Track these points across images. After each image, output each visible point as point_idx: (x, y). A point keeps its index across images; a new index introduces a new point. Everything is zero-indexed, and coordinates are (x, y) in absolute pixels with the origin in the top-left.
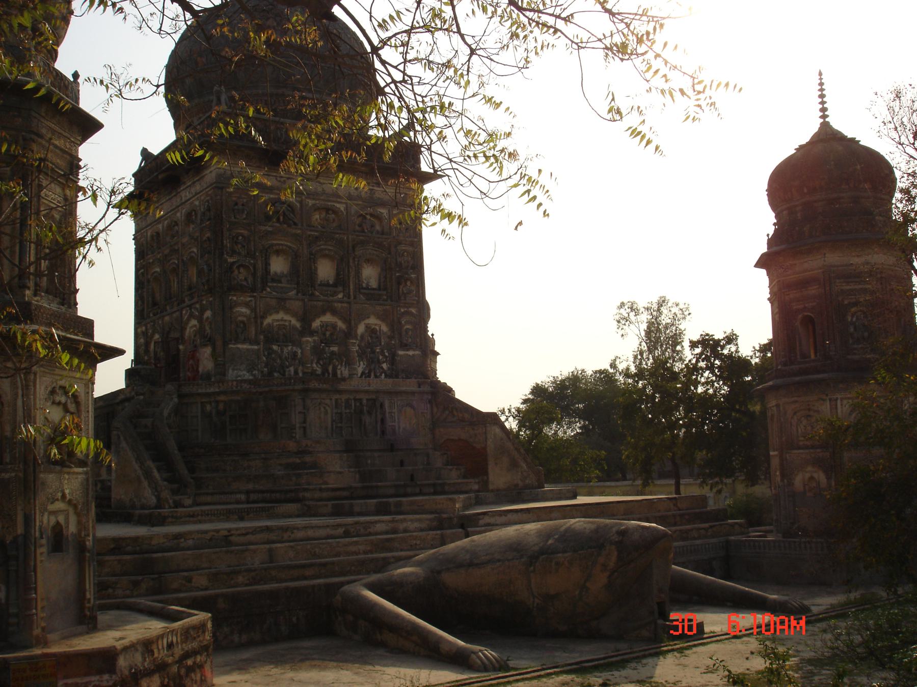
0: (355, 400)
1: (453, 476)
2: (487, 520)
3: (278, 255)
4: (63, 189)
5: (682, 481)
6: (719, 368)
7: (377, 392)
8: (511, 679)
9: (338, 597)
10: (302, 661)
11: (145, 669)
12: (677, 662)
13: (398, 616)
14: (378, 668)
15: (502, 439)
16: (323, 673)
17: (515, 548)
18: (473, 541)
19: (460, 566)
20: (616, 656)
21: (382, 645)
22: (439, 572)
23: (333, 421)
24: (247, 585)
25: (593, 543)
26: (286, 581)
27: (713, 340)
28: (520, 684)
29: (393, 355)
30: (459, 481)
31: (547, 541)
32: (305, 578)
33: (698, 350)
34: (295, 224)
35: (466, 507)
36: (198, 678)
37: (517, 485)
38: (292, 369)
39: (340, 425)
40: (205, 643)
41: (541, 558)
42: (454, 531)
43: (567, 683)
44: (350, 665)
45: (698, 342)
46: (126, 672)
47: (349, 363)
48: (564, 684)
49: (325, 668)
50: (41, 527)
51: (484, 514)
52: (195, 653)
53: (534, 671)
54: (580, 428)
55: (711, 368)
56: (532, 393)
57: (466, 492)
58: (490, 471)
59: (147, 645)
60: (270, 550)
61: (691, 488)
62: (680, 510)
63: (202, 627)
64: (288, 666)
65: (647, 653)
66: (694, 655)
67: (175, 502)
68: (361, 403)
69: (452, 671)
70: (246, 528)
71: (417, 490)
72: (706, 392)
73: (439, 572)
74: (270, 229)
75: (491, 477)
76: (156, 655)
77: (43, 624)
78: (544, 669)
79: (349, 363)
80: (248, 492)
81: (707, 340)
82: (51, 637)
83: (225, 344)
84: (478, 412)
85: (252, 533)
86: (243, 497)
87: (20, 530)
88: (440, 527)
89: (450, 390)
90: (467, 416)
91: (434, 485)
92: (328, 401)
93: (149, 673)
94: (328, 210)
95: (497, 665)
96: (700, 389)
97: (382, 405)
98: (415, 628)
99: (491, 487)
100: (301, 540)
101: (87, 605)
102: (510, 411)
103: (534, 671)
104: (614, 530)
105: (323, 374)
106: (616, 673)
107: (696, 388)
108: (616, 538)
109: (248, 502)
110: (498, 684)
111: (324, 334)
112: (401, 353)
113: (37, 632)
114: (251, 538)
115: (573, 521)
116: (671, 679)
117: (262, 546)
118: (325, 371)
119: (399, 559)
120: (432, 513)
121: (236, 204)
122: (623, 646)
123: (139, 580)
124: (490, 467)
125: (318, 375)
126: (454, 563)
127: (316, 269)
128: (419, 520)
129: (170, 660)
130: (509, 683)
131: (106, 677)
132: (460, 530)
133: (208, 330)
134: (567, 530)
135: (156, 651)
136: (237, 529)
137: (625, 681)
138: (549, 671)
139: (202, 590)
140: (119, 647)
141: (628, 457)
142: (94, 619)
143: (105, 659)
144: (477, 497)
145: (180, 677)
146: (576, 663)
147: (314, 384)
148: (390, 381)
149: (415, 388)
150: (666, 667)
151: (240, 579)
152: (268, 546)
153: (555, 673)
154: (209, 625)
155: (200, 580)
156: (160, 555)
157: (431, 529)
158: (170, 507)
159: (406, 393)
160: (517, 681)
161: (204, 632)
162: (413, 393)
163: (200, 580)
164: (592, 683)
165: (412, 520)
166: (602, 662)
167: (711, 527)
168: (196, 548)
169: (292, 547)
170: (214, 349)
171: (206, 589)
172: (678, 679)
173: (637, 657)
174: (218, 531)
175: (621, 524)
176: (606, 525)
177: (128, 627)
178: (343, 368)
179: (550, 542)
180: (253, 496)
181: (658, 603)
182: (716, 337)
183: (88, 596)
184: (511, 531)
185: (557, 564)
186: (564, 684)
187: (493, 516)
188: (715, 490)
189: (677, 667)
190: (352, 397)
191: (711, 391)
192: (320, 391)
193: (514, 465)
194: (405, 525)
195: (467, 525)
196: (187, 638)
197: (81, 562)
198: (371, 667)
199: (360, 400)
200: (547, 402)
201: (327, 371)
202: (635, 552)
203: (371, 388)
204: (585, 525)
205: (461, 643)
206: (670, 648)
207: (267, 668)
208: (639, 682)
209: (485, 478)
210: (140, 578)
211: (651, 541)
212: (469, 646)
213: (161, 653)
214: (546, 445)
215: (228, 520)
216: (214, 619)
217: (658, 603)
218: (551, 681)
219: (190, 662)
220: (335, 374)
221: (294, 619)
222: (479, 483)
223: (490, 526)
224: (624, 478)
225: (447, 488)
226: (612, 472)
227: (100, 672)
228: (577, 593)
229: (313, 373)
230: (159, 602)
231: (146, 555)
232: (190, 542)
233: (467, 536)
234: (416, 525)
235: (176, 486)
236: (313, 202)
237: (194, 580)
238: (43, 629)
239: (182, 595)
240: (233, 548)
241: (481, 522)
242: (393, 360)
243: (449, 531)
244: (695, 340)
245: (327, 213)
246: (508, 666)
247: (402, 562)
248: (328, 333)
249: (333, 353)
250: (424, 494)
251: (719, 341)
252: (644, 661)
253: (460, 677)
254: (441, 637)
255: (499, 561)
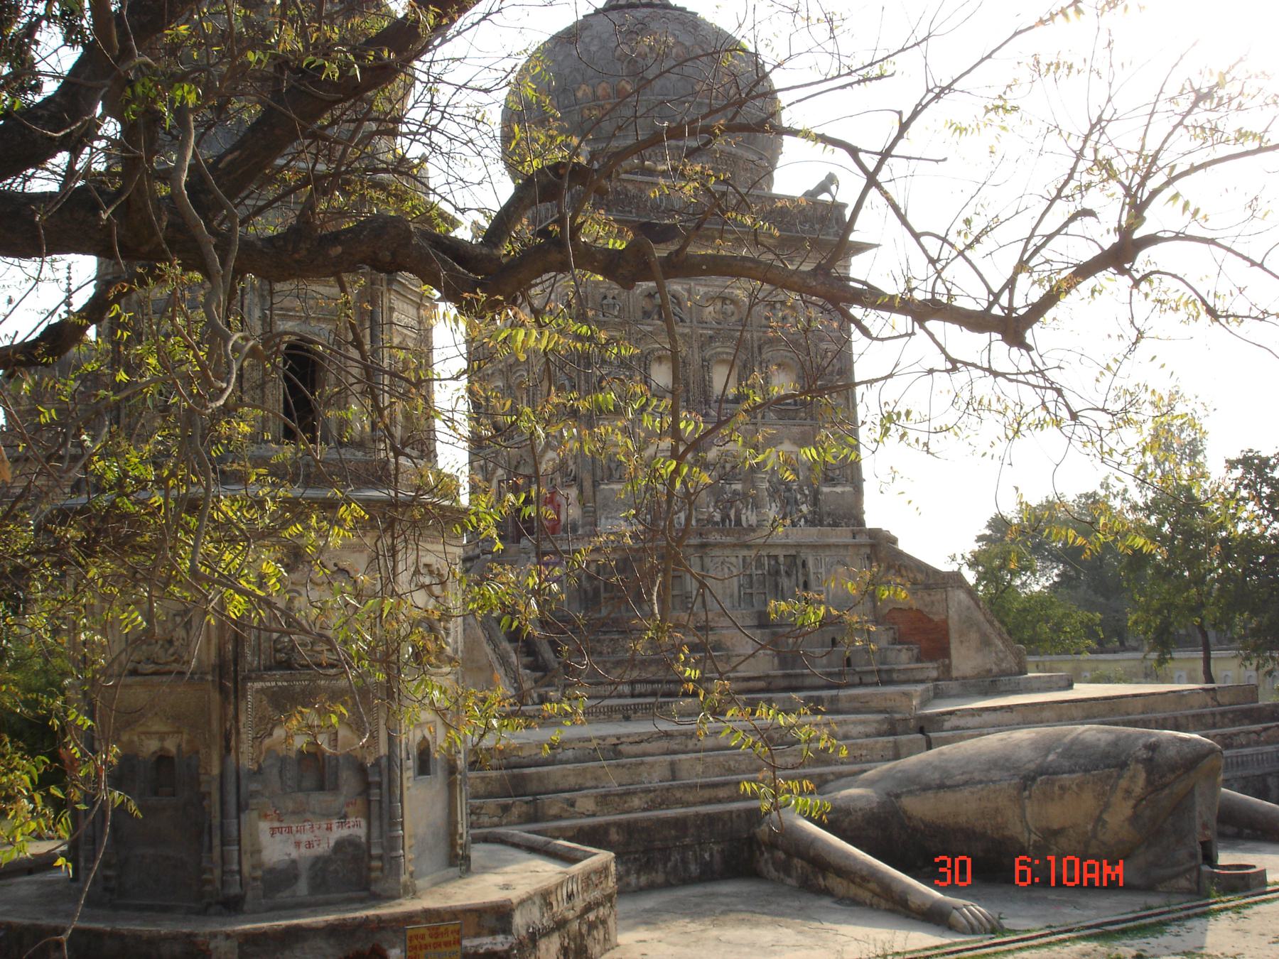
0: (769, 556)
1: (903, 658)
2: (954, 721)
3: (660, 362)
4: (418, 309)
5: (1213, 654)
6: (1268, 497)
7: (799, 545)
8: (1012, 946)
9: (764, 828)
10: (724, 913)
11: (545, 928)
12: (1234, 926)
13: (848, 856)
14: (827, 925)
15: (969, 608)
16: (756, 932)
17: (1001, 762)
18: (941, 753)
19: (926, 788)
20: (1149, 916)
21: (827, 892)
22: (898, 796)
23: (740, 586)
24: (644, 810)
25: (1110, 762)
26: (694, 804)
27: (1259, 458)
28: (1025, 954)
29: (816, 493)
30: (912, 666)
31: (1046, 756)
32: (719, 801)
33: (1238, 473)
34: (682, 321)
35: (924, 704)
36: (601, 937)
37: (990, 671)
38: (682, 515)
39: (749, 591)
40: (609, 891)
41: (1039, 779)
42: (911, 736)
43: (1088, 954)
44: (789, 920)
45: (1239, 461)
46: (523, 933)
47: (757, 505)
48: (1084, 955)
49: (757, 925)
50: (407, 744)
51: (951, 713)
52: (598, 904)
53: (1042, 936)
54: (1057, 575)
55: (1258, 498)
56: (989, 526)
57: (922, 681)
58: (953, 652)
59: (545, 897)
60: (672, 764)
61: (1231, 670)
62: (1219, 705)
63: (603, 871)
64: (707, 921)
65: (1191, 912)
66: (1256, 917)
67: (540, 696)
68: (777, 562)
69: (927, 932)
70: (639, 734)
71: (857, 680)
72: (1250, 531)
73: (898, 796)
74: (650, 329)
75: (955, 661)
76: (555, 909)
77: (411, 868)
78: (1053, 934)
79: (757, 505)
80: (632, 683)
81: (1250, 458)
82: (420, 883)
83: (595, 484)
84: (936, 572)
85: (648, 741)
86: (626, 689)
87: (383, 749)
88: (892, 732)
89: (880, 530)
90: (920, 577)
91: (879, 671)
92: (733, 560)
93: (547, 933)
94: (724, 299)
95: (988, 927)
96: (1241, 527)
97: (804, 564)
98: (874, 874)
99: (954, 674)
100: (712, 750)
101: (459, 841)
102: (963, 558)
103: (1042, 936)
104: (1141, 742)
105: (723, 520)
106: (1151, 940)
107: (1235, 526)
108: (1144, 754)
109: (633, 696)
110: (996, 953)
111: (724, 467)
112: (825, 490)
113: (404, 878)
114: (645, 747)
115: (1081, 728)
116: (1230, 951)
117: (661, 758)
118: (726, 517)
119: (839, 776)
120: (880, 712)
121: (605, 297)
122: (1154, 900)
123: (514, 801)
124: (953, 646)
125: (717, 523)
126: (919, 784)
127: (711, 381)
128: (863, 722)
129: (570, 915)
130: (1009, 951)
131: (500, 938)
132: (920, 736)
133: (572, 466)
134: (1073, 742)
135: (555, 903)
136: (628, 736)
137: (1166, 951)
138: (1061, 936)
139: (588, 816)
140: (515, 901)
141: (1136, 623)
142: (467, 859)
143: (499, 916)
144: (936, 687)
145: (582, 936)
146: (1097, 926)
147: (714, 537)
148: (814, 530)
149: (849, 540)
150: (1219, 932)
151: (636, 802)
152: (668, 758)
153: (1069, 939)
154: (613, 867)
155: (585, 803)
156: (533, 770)
157: (880, 734)
158: (534, 704)
159: (837, 546)
160: (1020, 949)
161: (606, 877)
162: (846, 546)
163: (585, 803)
164: (1122, 955)
165: (854, 723)
166: (1131, 924)
167: (1265, 729)
168: (577, 760)
169: (699, 759)
170: (581, 492)
171: (594, 815)
172: (1238, 951)
173: (1179, 919)
174: (604, 738)
175: (1150, 735)
176: (1129, 736)
177: (509, 869)
178: (749, 513)
179: (1051, 757)
180: (639, 688)
181: (1203, 844)
182: (1263, 455)
183: (460, 830)
184: (992, 742)
185: (1061, 787)
186: (1084, 955)
187: (962, 716)
188: (1262, 671)
189: (1236, 934)
190: (764, 553)
191: (1257, 531)
192: (723, 546)
193: (986, 642)
194: (845, 728)
195: (927, 730)
196: (588, 885)
197: (451, 786)
198: (816, 924)
199: (776, 557)
200: (1009, 542)
201: (728, 517)
202: (1169, 775)
203: (789, 541)
204: (1099, 736)
205: (937, 895)
206: (1222, 905)
207: (681, 922)
208: (1185, 953)
209: (947, 661)
210: (510, 801)
211: (1193, 761)
212: (948, 898)
213: (560, 907)
214: (1016, 605)
215: (609, 719)
216: (619, 857)
217: (1203, 844)
218: (1066, 950)
219: (592, 916)
220: (738, 522)
221: (707, 856)
222: (938, 668)
223: (960, 733)
224: (1124, 648)
225: (895, 676)
226: (1110, 638)
227: (493, 932)
228: (1090, 827)
229: (710, 520)
230: (529, 832)
231: (516, 771)
232: (570, 753)
233: (929, 747)
234: (861, 729)
235: (539, 674)
236: (706, 289)
237: (577, 804)
238: (411, 874)
239: (564, 823)
240: (624, 761)
241: (947, 725)
242: (815, 499)
243: (903, 738)
244: (1233, 458)
245: (724, 303)
246: (1002, 927)
247: (843, 781)
248: (728, 466)
249: (735, 493)
250: (866, 685)
251: (1268, 459)
252: (1189, 924)
253: (946, 941)
254: (909, 886)
255: (981, 782)
